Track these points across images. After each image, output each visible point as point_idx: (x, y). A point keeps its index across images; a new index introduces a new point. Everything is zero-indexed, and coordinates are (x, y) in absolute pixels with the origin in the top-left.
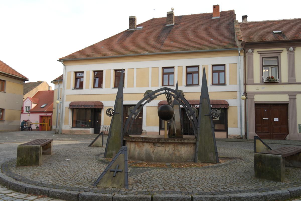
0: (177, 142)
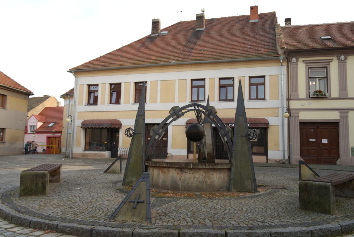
0: (208, 167)
